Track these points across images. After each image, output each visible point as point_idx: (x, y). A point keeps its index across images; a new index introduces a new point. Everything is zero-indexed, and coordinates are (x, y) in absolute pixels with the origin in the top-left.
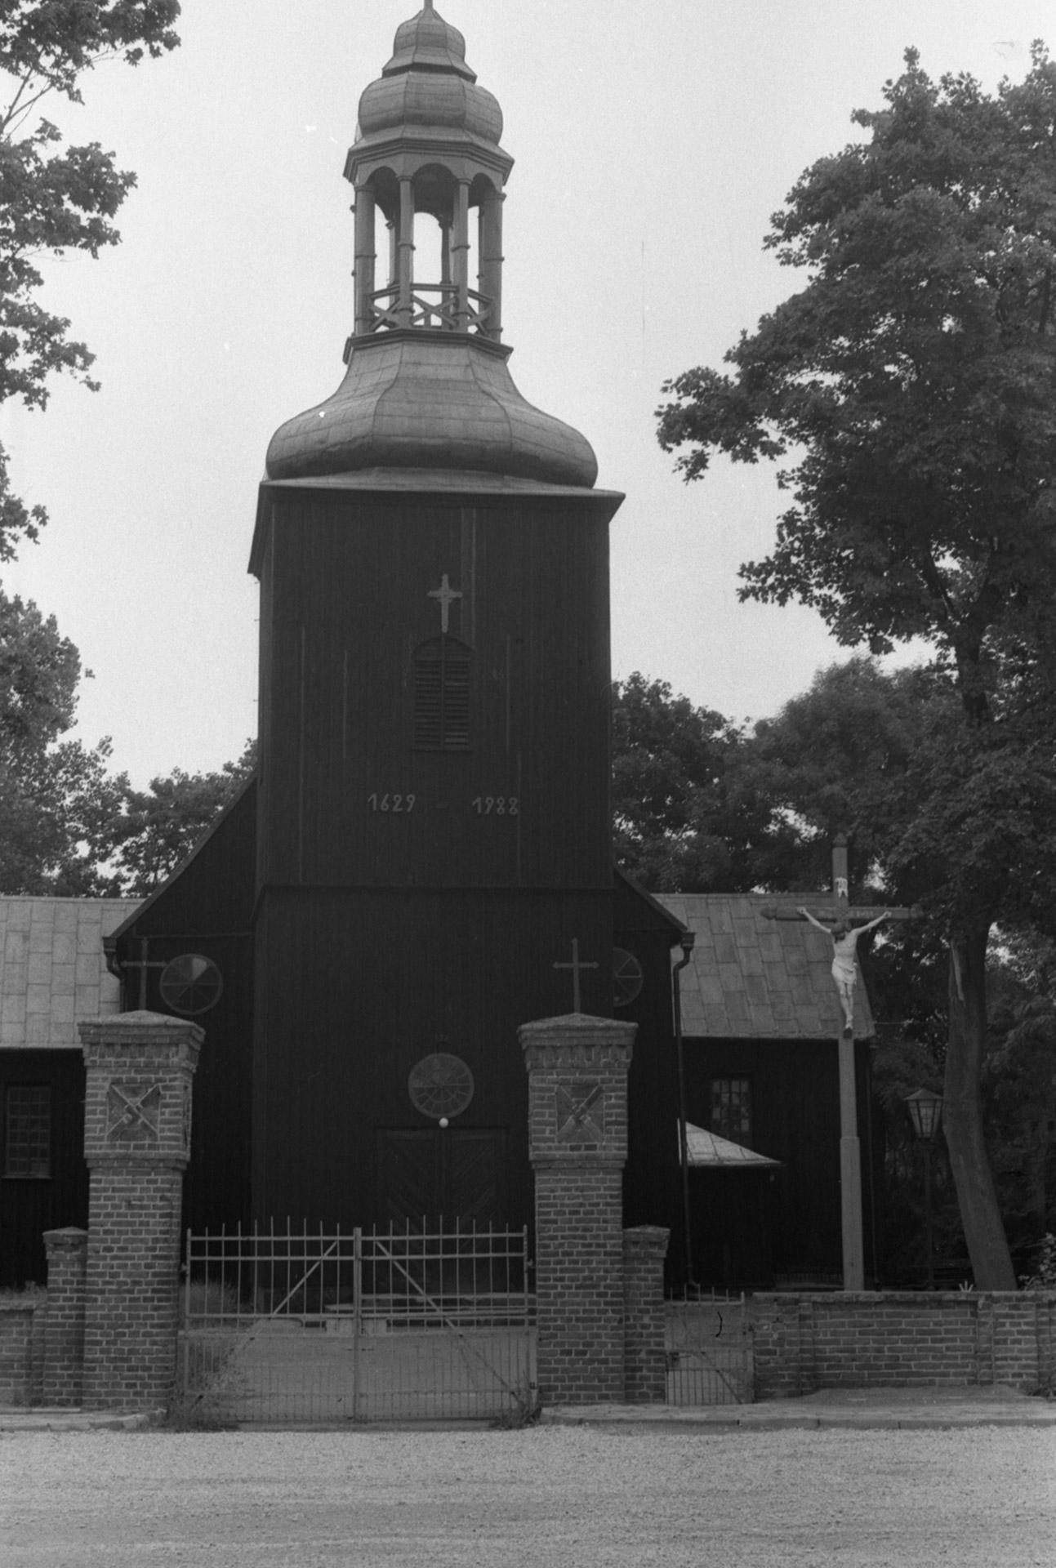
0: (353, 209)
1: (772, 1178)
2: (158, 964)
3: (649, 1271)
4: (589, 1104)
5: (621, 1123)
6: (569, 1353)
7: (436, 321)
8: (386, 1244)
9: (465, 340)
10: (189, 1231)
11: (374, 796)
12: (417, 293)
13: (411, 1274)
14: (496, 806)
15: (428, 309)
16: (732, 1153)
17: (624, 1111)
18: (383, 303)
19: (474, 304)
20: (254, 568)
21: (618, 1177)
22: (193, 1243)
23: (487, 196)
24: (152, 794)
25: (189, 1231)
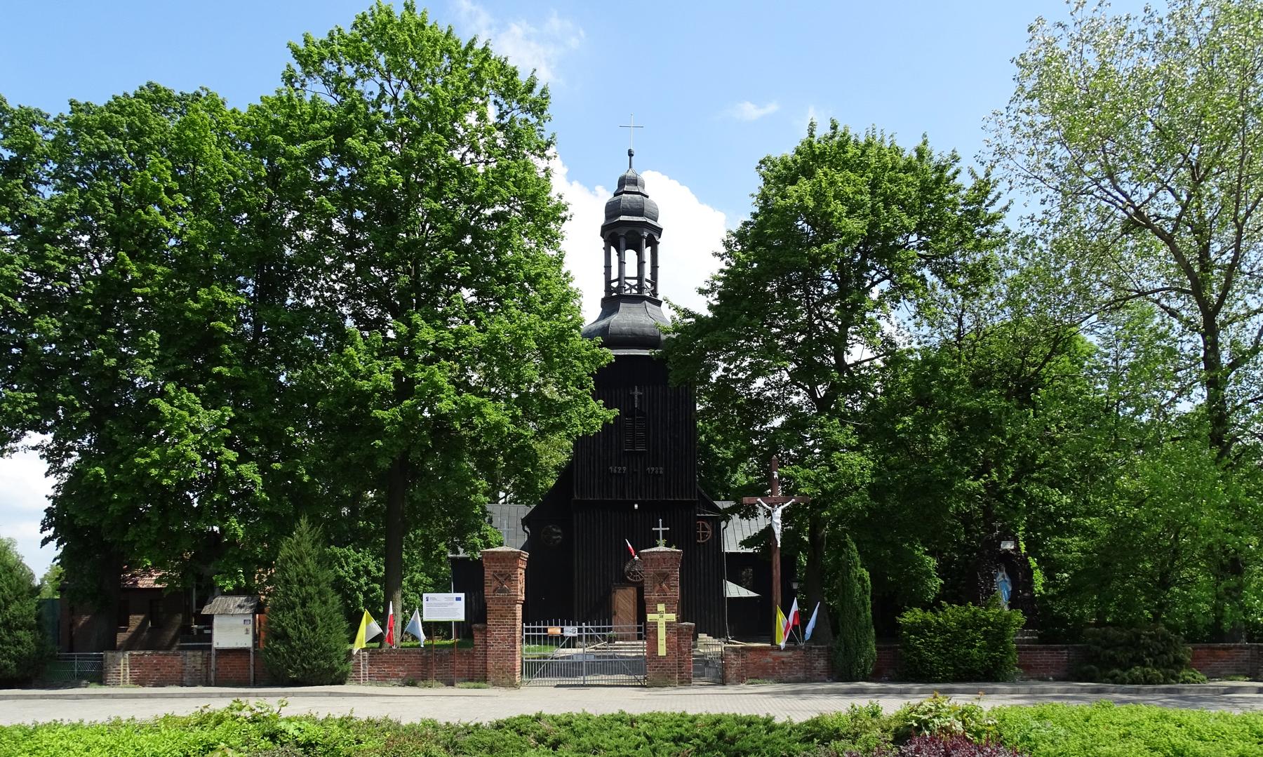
2: (518, 663)
7: (634, 291)
9: (645, 298)
15: (632, 287)
16: (744, 593)
19: (649, 285)
23: (653, 244)
24: (710, 315)
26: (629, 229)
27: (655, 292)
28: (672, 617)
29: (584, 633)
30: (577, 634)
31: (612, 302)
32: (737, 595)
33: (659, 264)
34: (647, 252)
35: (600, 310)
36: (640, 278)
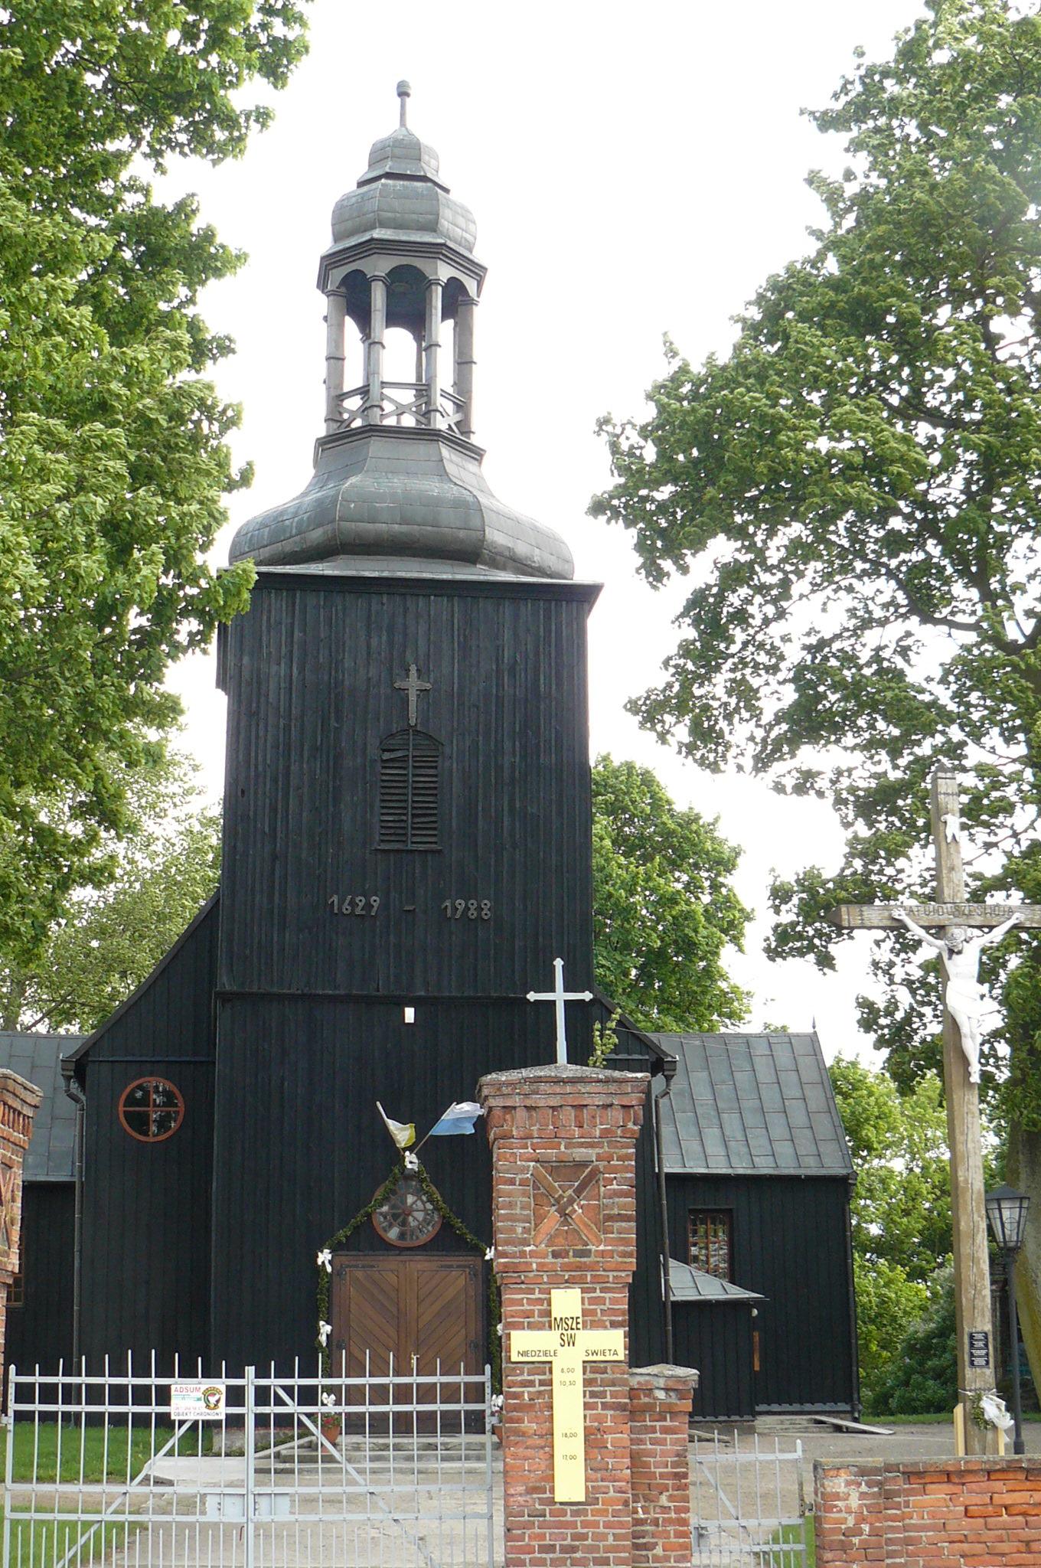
0: (325, 318)
1: (755, 1312)
3: (665, 1430)
4: (579, 1191)
5: (627, 1219)
6: (551, 1549)
8: (289, 1390)
9: (435, 435)
10: (12, 1367)
11: (335, 898)
12: (385, 391)
13: (323, 1433)
14: (467, 908)
17: (631, 1201)
18: (354, 403)
19: (449, 407)
20: (222, 682)
21: (625, 1295)
22: (19, 1386)
23: (458, 302)
25: (12, 1367)
26: (395, 267)
27: (464, 425)
28: (613, 1343)
29: (250, 1410)
30: (222, 1412)
31: (345, 441)
32: (691, 1296)
33: (477, 355)
34: (444, 331)
35: (312, 472)
36: (423, 389)
